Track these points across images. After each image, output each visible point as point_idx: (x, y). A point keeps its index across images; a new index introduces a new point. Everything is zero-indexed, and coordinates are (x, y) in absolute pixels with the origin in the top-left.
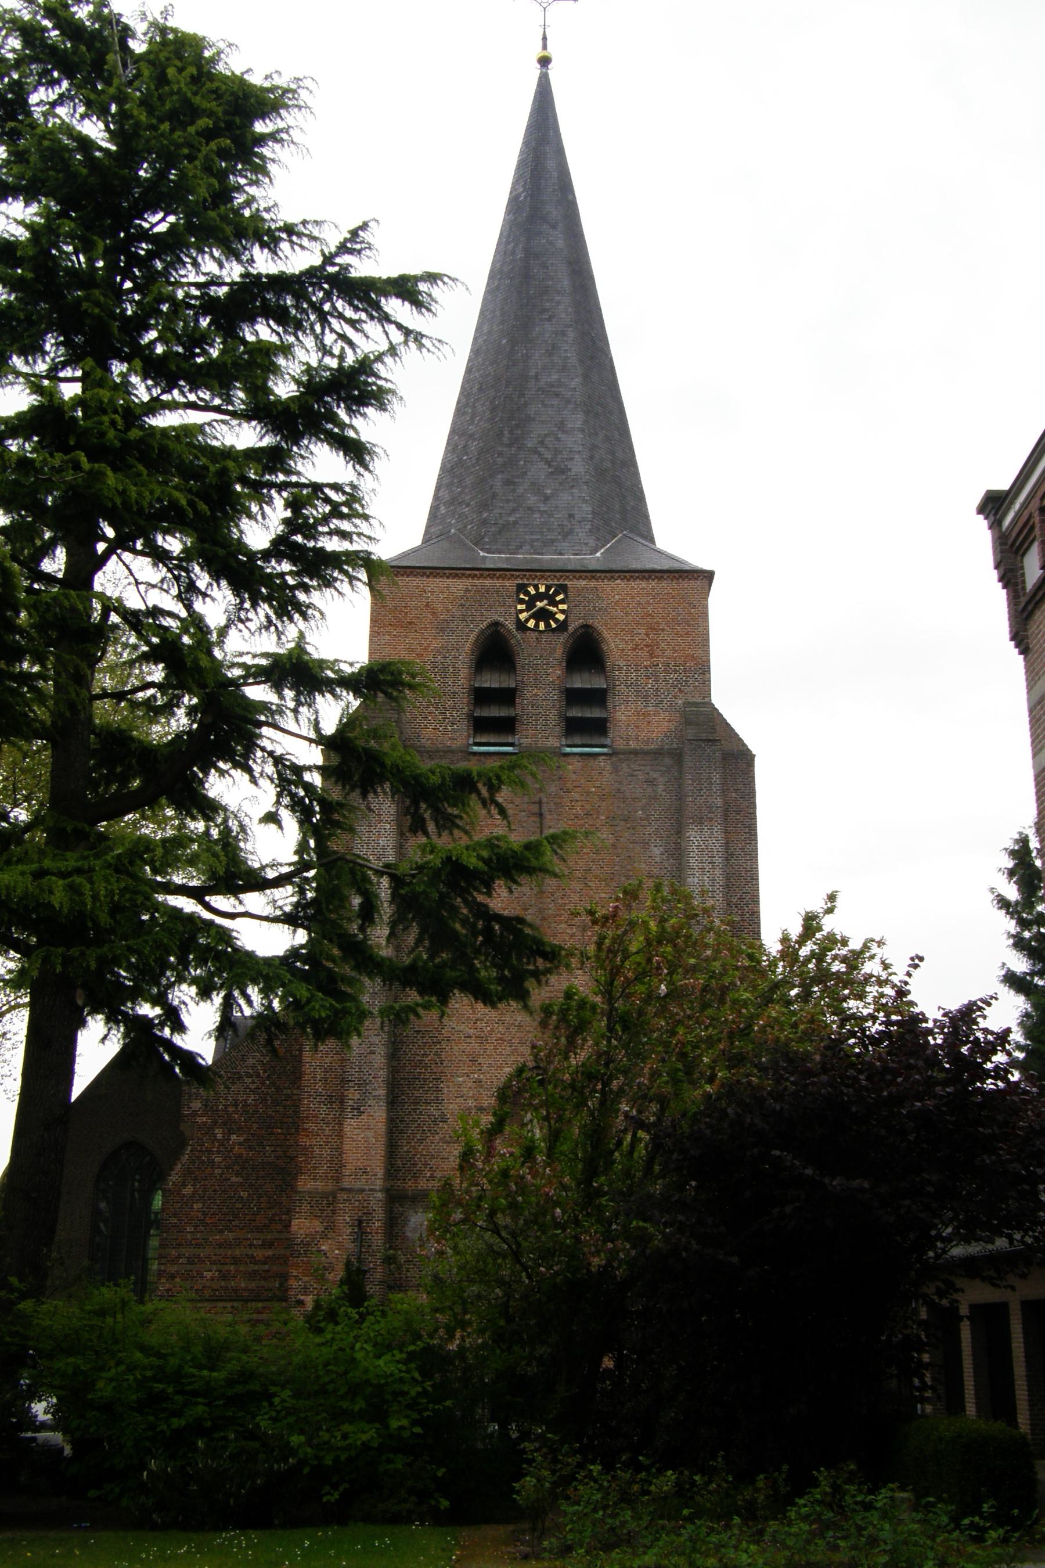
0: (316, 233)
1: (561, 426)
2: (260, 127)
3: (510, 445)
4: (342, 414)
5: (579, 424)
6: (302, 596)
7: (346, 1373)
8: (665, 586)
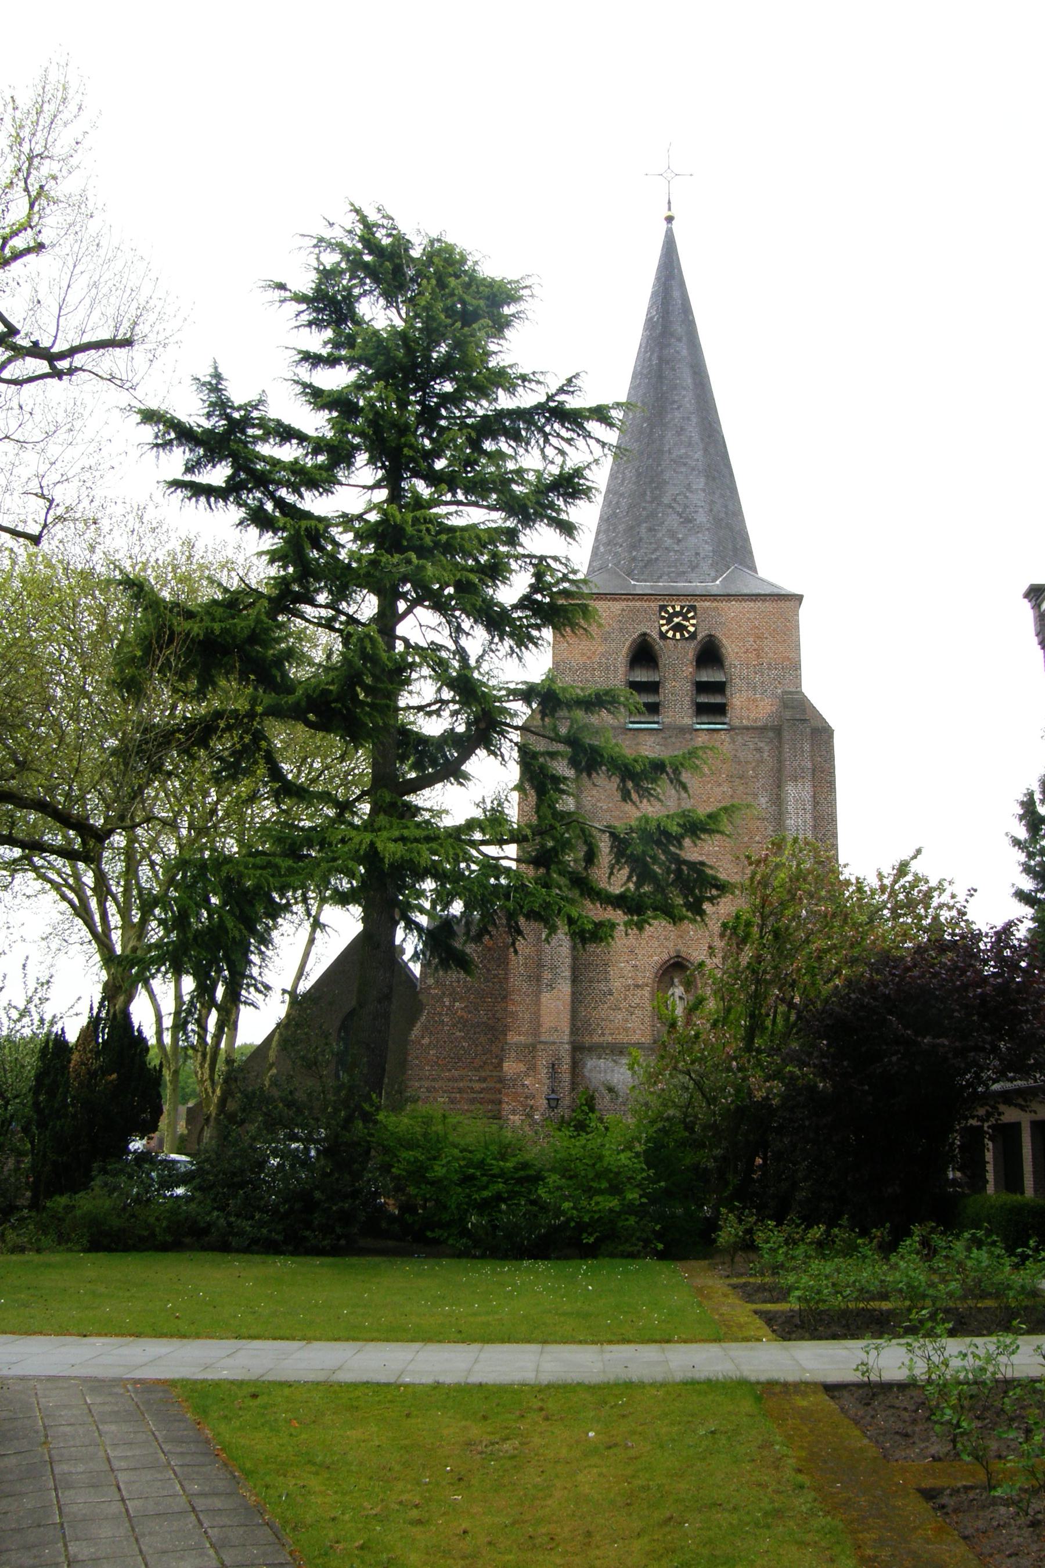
0: (541, 379)
1: (689, 487)
2: (507, 310)
3: (651, 502)
4: (560, 502)
5: (701, 486)
6: (535, 633)
7: (594, 1165)
8: (768, 606)
